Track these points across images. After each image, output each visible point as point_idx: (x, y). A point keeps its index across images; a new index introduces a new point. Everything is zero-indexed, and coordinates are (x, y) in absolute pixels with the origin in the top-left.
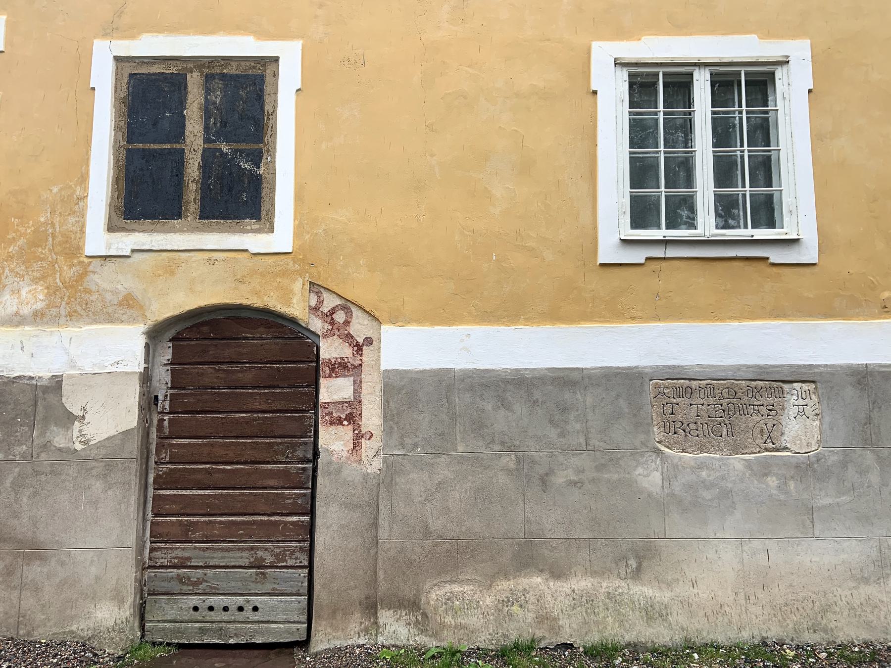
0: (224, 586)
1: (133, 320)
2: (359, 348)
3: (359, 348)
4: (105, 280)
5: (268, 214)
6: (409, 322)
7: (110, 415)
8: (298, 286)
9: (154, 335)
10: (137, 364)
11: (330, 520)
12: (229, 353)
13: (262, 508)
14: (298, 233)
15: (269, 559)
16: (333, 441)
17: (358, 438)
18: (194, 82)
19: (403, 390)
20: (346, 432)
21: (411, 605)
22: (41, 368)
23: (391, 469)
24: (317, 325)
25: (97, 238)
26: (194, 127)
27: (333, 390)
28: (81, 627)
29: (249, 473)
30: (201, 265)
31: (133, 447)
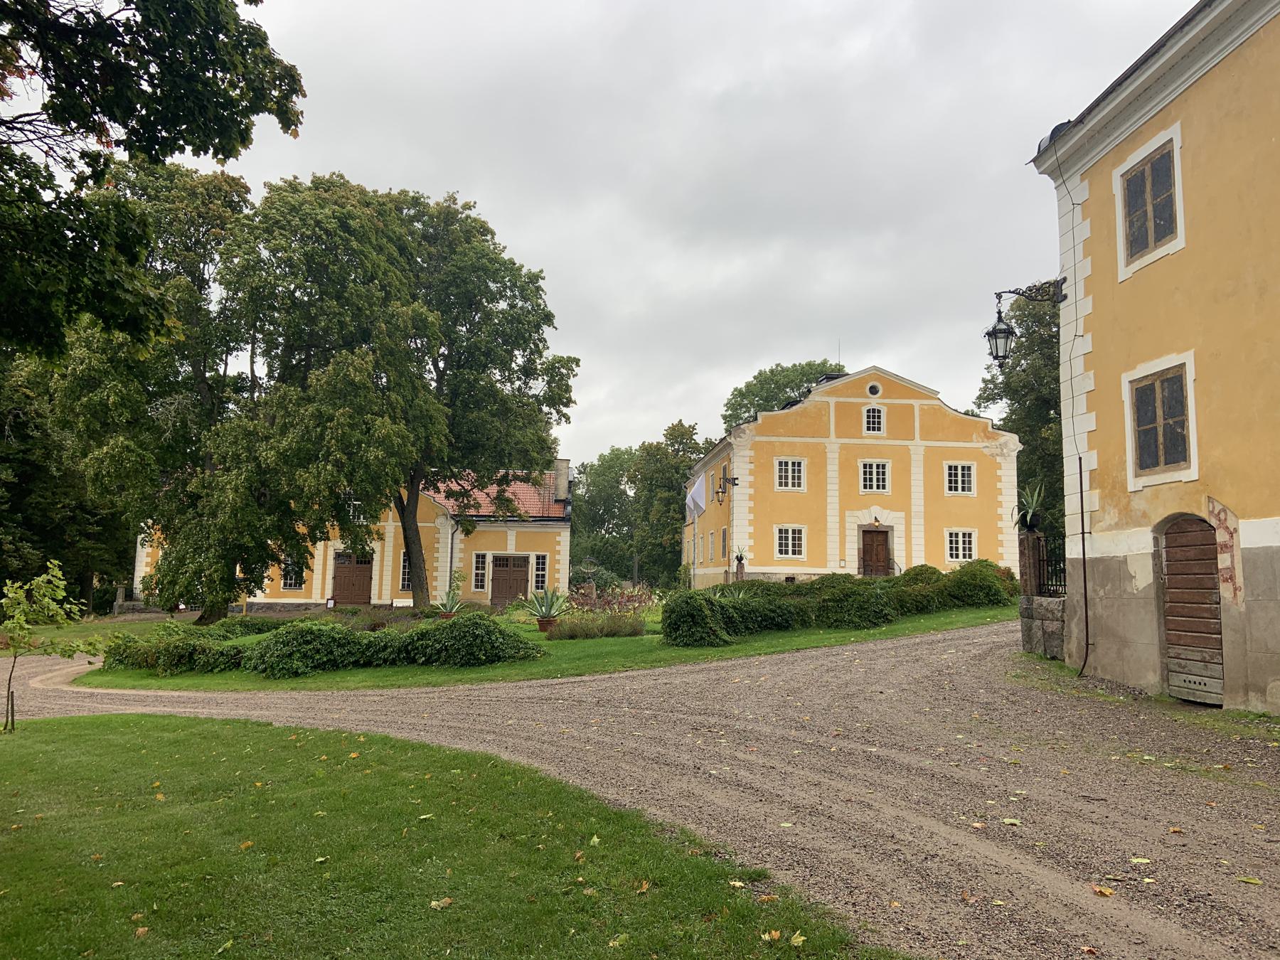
0: (1194, 671)
1: (1147, 525)
2: (1231, 534)
3: (1231, 534)
4: (1138, 504)
5: (673, 658)
6: (1249, 517)
7: (1143, 577)
8: (1204, 499)
9: (1157, 529)
10: (1151, 549)
11: (1227, 636)
12: (1184, 541)
13: (1203, 629)
14: (1200, 469)
15: (1208, 658)
16: (1225, 591)
17: (1235, 589)
18: (1158, 385)
19: (1256, 559)
20: (1229, 585)
21: (1262, 691)
22: (1119, 552)
23: (1249, 610)
24: (1214, 522)
25: (1133, 483)
26: (1159, 412)
27: (1223, 561)
28: (1143, 683)
29: (1196, 609)
30: (1172, 489)
31: (1152, 593)
